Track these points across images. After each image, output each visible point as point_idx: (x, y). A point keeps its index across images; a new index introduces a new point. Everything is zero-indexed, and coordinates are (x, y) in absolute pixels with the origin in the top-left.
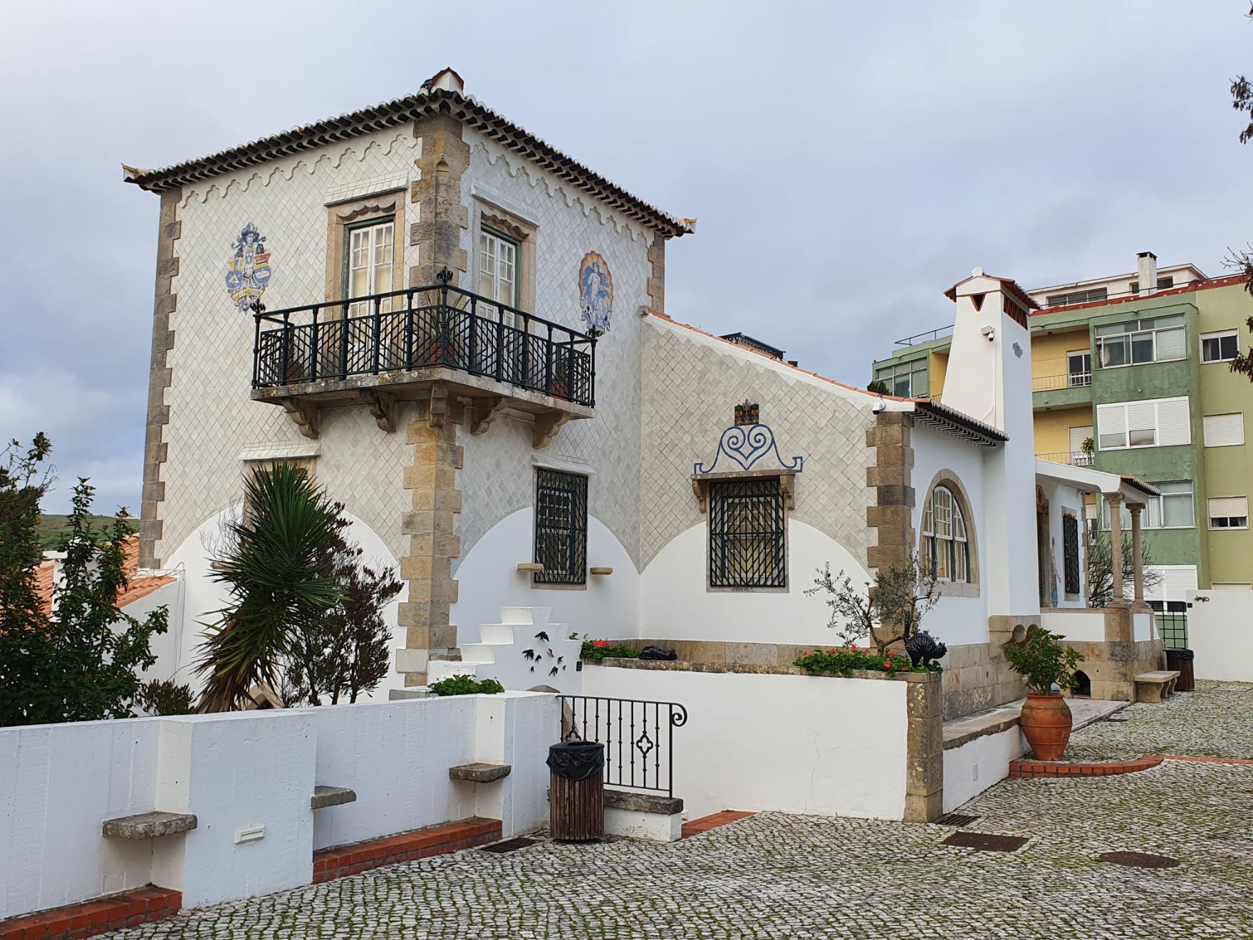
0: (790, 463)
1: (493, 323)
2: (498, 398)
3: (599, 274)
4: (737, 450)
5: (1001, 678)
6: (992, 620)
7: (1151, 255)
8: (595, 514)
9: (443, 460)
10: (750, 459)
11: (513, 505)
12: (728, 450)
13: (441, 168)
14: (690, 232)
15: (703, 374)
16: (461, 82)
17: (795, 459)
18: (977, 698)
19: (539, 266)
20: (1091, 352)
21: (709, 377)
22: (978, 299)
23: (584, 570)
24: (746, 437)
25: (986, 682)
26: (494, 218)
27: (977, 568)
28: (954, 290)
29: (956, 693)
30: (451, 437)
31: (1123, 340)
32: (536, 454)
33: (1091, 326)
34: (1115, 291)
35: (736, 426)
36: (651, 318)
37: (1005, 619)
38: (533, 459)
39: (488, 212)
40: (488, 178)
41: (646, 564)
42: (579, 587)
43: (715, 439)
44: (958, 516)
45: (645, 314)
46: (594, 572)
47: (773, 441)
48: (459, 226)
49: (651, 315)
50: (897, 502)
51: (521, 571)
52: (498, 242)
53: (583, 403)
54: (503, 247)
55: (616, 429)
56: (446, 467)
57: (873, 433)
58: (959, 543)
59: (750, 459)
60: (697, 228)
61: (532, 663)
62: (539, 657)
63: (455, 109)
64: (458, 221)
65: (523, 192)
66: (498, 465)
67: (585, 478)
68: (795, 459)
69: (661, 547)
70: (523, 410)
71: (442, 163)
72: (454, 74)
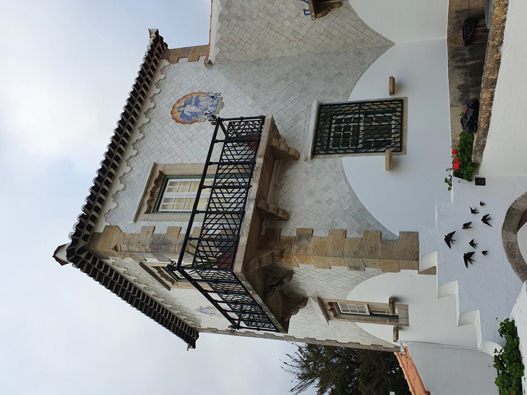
1: (206, 219)
2: (257, 209)
3: (184, 106)
8: (348, 94)
9: (306, 248)
11: (341, 175)
13: (119, 249)
14: (157, 33)
15: (238, 18)
16: (59, 248)
19: (179, 161)
23: (391, 101)
26: (150, 207)
30: (290, 241)
32: (302, 157)
36: (211, 58)
38: (306, 160)
39: (145, 208)
40: (123, 212)
41: (387, 40)
42: (405, 102)
45: (210, 62)
46: (392, 93)
48: (152, 236)
49: (209, 58)
51: (392, 165)
52: (166, 195)
53: (263, 123)
54: (170, 190)
55: (286, 80)
56: (311, 245)
60: (154, 27)
61: (478, 256)
62: (472, 244)
63: (82, 243)
64: (149, 236)
65: (136, 175)
66: (311, 193)
67: (321, 107)
69: (372, 31)
70: (271, 176)
71: (116, 249)
72: (56, 252)
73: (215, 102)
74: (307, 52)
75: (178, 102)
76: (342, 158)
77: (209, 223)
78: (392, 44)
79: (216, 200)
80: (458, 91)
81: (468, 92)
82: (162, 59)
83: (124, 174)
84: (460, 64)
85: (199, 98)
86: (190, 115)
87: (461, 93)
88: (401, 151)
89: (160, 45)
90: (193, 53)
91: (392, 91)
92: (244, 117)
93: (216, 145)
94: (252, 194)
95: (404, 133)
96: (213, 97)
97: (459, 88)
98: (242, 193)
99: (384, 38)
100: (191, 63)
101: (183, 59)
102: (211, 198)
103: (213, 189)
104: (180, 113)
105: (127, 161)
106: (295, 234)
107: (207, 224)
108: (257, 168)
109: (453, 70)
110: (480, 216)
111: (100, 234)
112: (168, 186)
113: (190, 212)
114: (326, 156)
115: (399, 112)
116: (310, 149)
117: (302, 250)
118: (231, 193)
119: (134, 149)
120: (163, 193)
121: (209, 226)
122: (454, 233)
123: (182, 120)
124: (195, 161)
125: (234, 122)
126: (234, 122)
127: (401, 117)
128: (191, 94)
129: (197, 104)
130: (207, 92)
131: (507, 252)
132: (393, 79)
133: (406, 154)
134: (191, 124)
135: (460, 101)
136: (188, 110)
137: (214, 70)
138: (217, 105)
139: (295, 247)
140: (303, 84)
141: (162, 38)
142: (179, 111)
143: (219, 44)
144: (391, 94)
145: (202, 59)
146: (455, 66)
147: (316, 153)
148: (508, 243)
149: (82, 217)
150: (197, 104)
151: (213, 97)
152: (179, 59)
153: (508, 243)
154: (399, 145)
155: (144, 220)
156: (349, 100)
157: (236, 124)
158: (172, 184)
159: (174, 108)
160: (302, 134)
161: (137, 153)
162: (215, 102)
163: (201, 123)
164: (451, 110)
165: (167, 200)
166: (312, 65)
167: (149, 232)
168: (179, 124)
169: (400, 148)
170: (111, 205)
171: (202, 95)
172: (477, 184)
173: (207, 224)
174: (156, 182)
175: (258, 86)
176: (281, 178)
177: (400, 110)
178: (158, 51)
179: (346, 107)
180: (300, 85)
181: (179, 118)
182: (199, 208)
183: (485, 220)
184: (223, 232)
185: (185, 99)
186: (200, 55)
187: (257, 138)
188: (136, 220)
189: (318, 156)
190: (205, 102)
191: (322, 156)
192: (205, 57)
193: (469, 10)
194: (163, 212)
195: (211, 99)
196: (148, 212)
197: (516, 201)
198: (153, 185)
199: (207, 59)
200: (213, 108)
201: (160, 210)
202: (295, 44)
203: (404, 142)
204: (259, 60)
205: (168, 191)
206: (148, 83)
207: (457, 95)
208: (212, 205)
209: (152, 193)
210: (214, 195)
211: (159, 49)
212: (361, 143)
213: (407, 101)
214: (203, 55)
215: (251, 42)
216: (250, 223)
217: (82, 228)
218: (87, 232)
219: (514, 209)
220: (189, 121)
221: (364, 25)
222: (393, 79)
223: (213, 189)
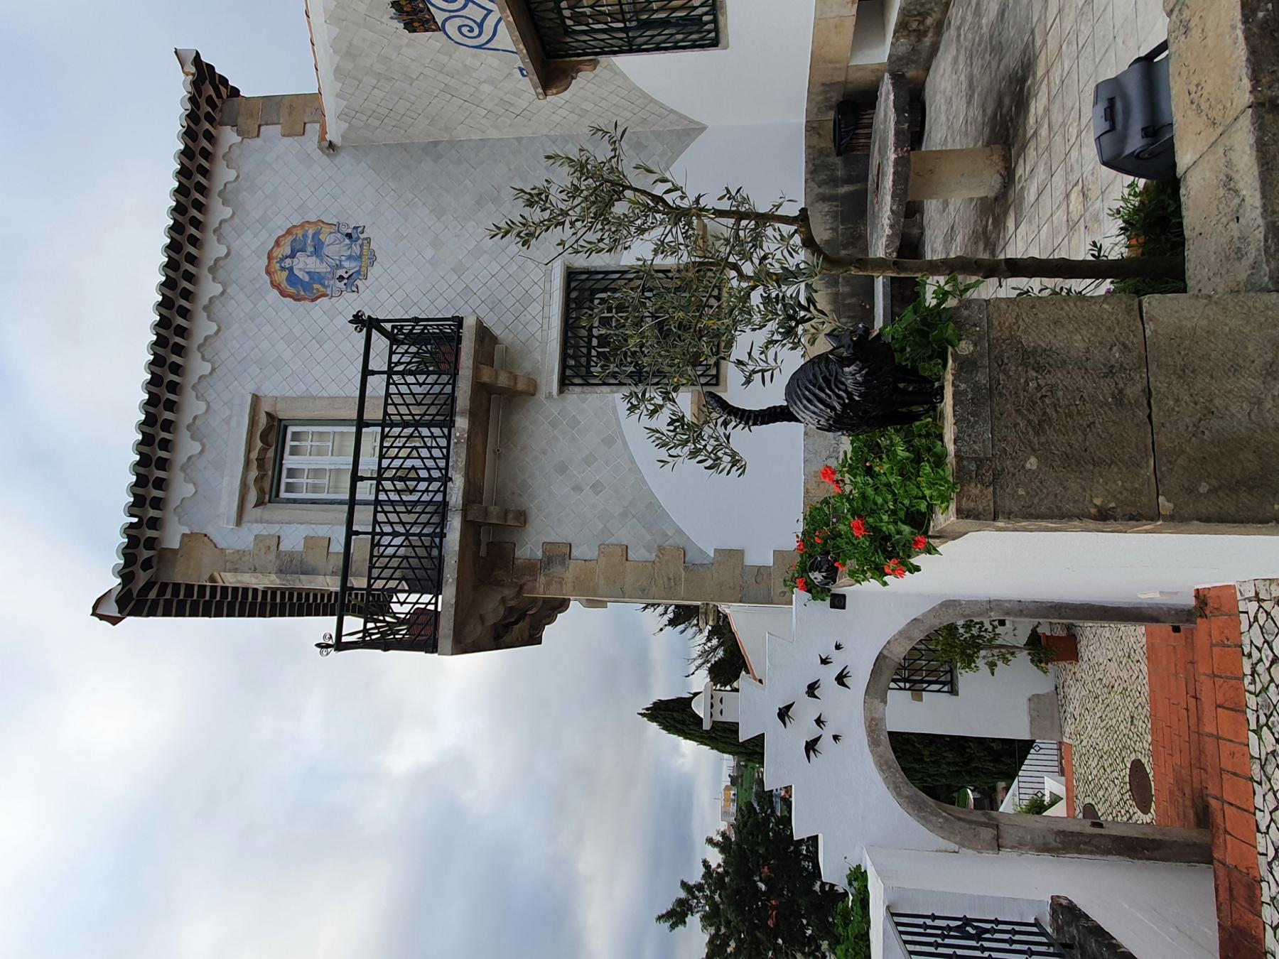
1: (384, 437)
3: (292, 256)
4: (480, 25)
12: (484, 38)
15: (379, 76)
19: (300, 389)
24: (454, 14)
26: (261, 492)
35: (442, 29)
39: (253, 496)
43: (474, 56)
45: (331, 145)
48: (279, 554)
52: (289, 462)
54: (295, 451)
61: (826, 743)
62: (819, 722)
63: (142, 577)
64: (272, 555)
69: (662, 106)
72: (95, 607)
75: (277, 243)
77: (391, 447)
78: (703, 128)
79: (398, 400)
82: (222, 124)
83: (195, 418)
84: (826, 190)
85: (322, 237)
86: (306, 278)
89: (212, 92)
90: (290, 114)
93: (371, 380)
94: (454, 499)
96: (349, 236)
98: (445, 385)
99: (685, 117)
102: (388, 395)
104: (285, 274)
105: (194, 387)
106: (539, 554)
107: (389, 448)
110: (834, 670)
111: (174, 551)
112: (289, 443)
113: (341, 502)
116: (555, 378)
117: (554, 585)
118: (424, 383)
119: (203, 358)
120: (282, 459)
121: (393, 452)
122: (791, 705)
123: (293, 290)
124: (333, 390)
128: (302, 225)
129: (318, 250)
131: (869, 736)
134: (313, 300)
136: (301, 265)
137: (344, 158)
138: (360, 257)
139: (542, 579)
141: (211, 68)
142: (283, 269)
146: (817, 195)
148: (872, 719)
149: (130, 530)
150: (318, 250)
151: (349, 236)
153: (872, 719)
155: (256, 521)
156: (622, 263)
158: (296, 436)
159: (270, 258)
161: (213, 370)
165: (292, 473)
167: (269, 548)
168: (288, 299)
170: (181, 489)
171: (326, 229)
172: (833, 606)
173: (389, 448)
174: (264, 437)
176: (508, 435)
178: (210, 97)
181: (284, 284)
182: (367, 416)
183: (841, 679)
184: (410, 552)
185: (290, 238)
188: (239, 521)
190: (335, 248)
191: (578, 389)
193: (846, 81)
194: (289, 501)
195: (347, 241)
196: (260, 503)
197: (889, 642)
198: (259, 444)
200: (353, 264)
201: (283, 495)
204: (436, 143)
205: (292, 454)
208: (391, 410)
209: (261, 461)
210: (393, 389)
211: (210, 101)
215: (415, 116)
216: (456, 558)
217: (137, 546)
218: (147, 554)
219: (885, 657)
220: (308, 295)
221: (644, 95)
223: (379, 483)
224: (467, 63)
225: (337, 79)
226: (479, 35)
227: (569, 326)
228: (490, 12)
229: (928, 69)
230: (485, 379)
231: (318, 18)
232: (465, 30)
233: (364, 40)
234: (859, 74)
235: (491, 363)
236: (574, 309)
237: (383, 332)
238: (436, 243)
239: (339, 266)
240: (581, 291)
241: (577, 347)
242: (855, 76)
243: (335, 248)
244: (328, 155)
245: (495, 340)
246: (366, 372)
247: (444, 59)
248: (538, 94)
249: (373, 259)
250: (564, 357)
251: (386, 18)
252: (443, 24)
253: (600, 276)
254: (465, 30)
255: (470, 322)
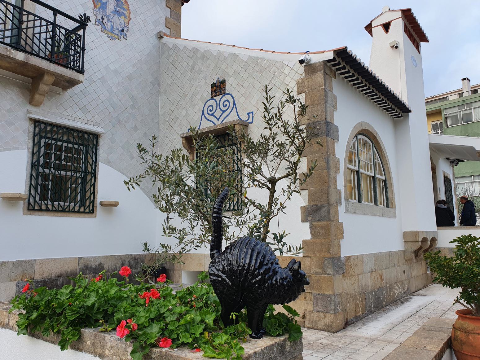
0: (244, 118)
4: (212, 115)
5: (414, 273)
6: (405, 234)
7: (468, 79)
8: (108, 162)
10: (220, 120)
12: (207, 116)
15: (193, 67)
17: (248, 114)
18: (397, 290)
20: (443, 120)
21: (197, 68)
22: (386, 27)
24: (218, 104)
25: (404, 277)
27: (393, 198)
28: (370, 25)
29: (381, 289)
31: (458, 114)
33: (442, 109)
34: (451, 98)
35: (212, 98)
37: (416, 233)
38: (29, 112)
42: (90, 215)
44: (378, 161)
45: (161, 37)
46: (102, 204)
47: (234, 104)
49: (165, 37)
50: (322, 134)
53: (78, 71)
57: (302, 82)
58: (380, 180)
59: (220, 120)
67: (96, 136)
68: (248, 114)
70: (7, 69)
73: (116, 32)
74: (160, 130)
76: (26, 150)
80: (97, 264)
81: (94, 273)
85: (123, 17)
87: (94, 266)
88: (29, 209)
91: (103, 203)
92: (85, 52)
93: (51, 13)
95: (52, 213)
97: (100, 265)
100: (164, 20)
101: (170, 13)
103: (52, 24)
108: (10, 51)
109: (121, 259)
114: (32, 134)
115: (79, 210)
125: (80, 41)
126: (80, 41)
127: (73, 211)
128: (129, 10)
130: (129, 26)
132: (116, 204)
133: (24, 214)
135: (84, 267)
137: (155, 41)
138: (112, 32)
140: (126, 122)
143: (175, 46)
144: (101, 202)
145: (167, 31)
146: (125, 261)
147: (37, 124)
151: (123, 31)
152: (170, 8)
154: (36, 208)
156: (100, 163)
157: (79, 43)
160: (65, 113)
162: (116, 32)
163: (92, 11)
164: (76, 258)
166: (145, 133)
169: (31, 209)
171: (126, 21)
175: (130, 78)
177: (82, 210)
179: (93, 160)
180: (125, 119)
182: (59, 16)
186: (171, 30)
187: (53, 60)
189: (33, 125)
190: (117, 22)
191: (32, 129)
192: (169, 34)
195: (120, 29)
199: (165, 34)
202: (167, 120)
203: (40, 213)
204: (159, 85)
206: (353, 84)
207: (92, 263)
208: (31, 17)
212: (44, 171)
213: (92, 217)
214: (170, 33)
215: (173, 78)
222: (116, 204)
223: (52, 24)
224: (196, 106)
225: (193, 49)
226: (208, 114)
227: (69, 130)
228: (218, 120)
229: (337, 332)
230: (46, 78)
231: (221, 48)
232: (211, 108)
233: (210, 65)
234: (177, 276)
235: (55, 84)
236: (78, 135)
237: (77, 29)
238: (116, 72)
239: (109, 19)
240: (88, 140)
241: (57, 133)
242: (176, 274)
243: (117, 22)
244: (157, 34)
245: (65, 88)
246: (56, 12)
247: (199, 97)
248: (183, 134)
249: (112, 39)
250: (52, 125)
251: (218, 76)
252: (214, 99)
253: (94, 151)
254: (211, 108)
255: (80, 77)
